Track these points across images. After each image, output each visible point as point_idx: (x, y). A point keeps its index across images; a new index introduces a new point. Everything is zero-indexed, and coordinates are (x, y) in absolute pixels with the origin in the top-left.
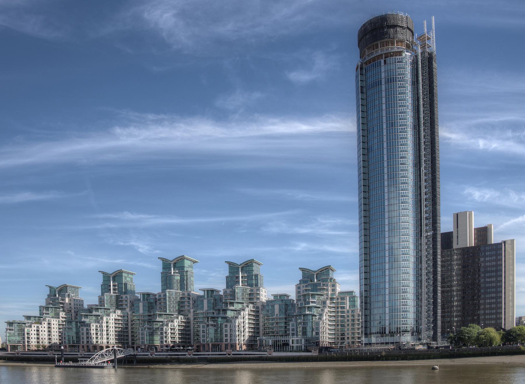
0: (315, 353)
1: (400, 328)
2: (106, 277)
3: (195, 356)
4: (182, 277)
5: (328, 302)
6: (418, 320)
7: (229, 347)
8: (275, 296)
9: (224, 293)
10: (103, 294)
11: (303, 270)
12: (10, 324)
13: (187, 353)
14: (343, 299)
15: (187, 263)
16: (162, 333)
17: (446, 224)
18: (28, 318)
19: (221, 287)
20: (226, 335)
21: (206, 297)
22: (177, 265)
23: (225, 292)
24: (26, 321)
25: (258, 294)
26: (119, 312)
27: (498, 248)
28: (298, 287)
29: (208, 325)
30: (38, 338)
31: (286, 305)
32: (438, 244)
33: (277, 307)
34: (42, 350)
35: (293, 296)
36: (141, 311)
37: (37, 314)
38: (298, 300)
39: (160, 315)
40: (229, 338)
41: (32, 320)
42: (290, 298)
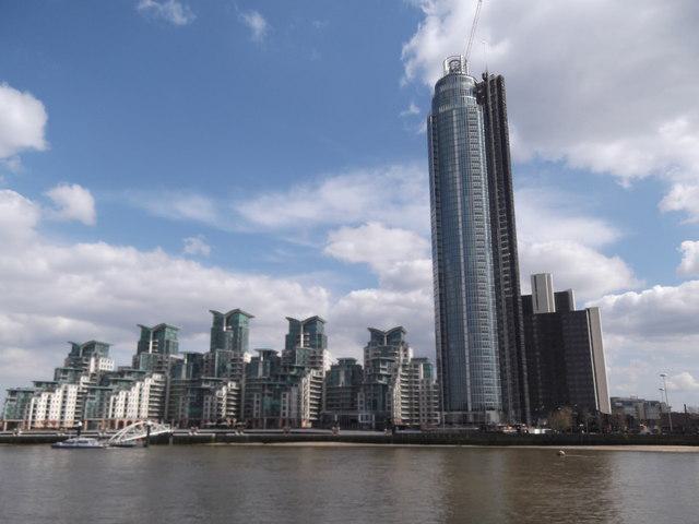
0: (386, 433)
2: (145, 332)
4: (235, 336)
5: (400, 370)
6: (503, 397)
7: (287, 422)
8: (341, 361)
10: (139, 353)
12: (13, 393)
14: (416, 366)
15: (242, 318)
17: (525, 289)
18: (38, 384)
19: (279, 348)
20: (284, 408)
24: (35, 388)
25: (321, 358)
26: (157, 377)
27: (582, 315)
28: (367, 351)
29: (263, 395)
30: (47, 412)
31: (272, 363)
32: (515, 308)
34: (42, 429)
35: (361, 362)
36: (183, 376)
37: (51, 379)
38: (366, 366)
39: (207, 381)
40: (287, 411)
41: (44, 387)
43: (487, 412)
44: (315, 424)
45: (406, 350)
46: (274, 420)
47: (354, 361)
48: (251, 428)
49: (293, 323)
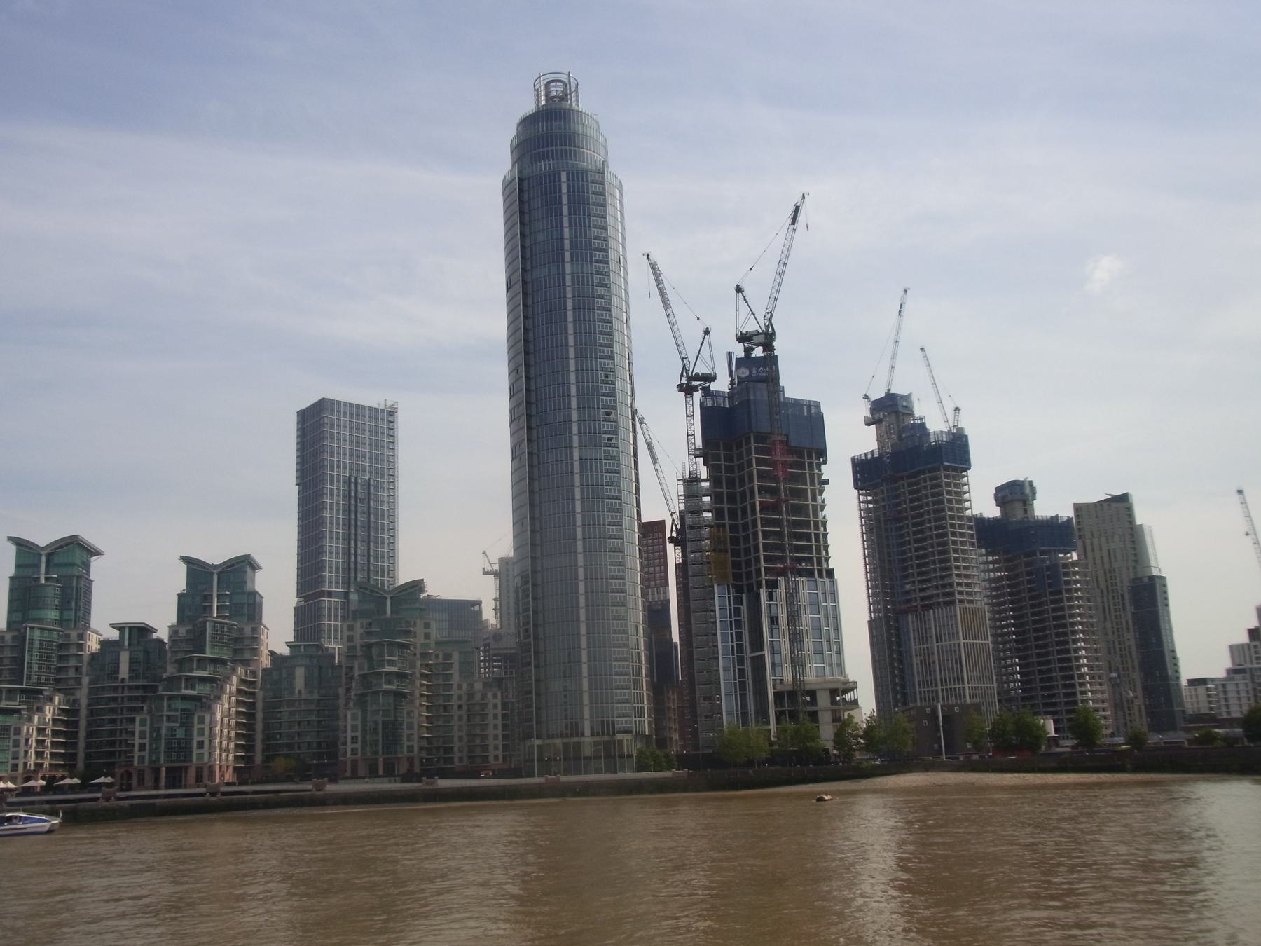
1: (613, 723)
3: (122, 803)
9: (170, 637)
11: (188, 561)
13: (99, 795)
16: (16, 744)
21: (126, 643)
22: (56, 560)
23: (173, 631)
33: (300, 673)
42: (155, 636)
43: (619, 737)
44: (242, 774)
45: (427, 625)
46: (180, 768)
47: (1145, 600)
48: (129, 788)
49: (195, 568)
